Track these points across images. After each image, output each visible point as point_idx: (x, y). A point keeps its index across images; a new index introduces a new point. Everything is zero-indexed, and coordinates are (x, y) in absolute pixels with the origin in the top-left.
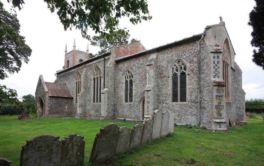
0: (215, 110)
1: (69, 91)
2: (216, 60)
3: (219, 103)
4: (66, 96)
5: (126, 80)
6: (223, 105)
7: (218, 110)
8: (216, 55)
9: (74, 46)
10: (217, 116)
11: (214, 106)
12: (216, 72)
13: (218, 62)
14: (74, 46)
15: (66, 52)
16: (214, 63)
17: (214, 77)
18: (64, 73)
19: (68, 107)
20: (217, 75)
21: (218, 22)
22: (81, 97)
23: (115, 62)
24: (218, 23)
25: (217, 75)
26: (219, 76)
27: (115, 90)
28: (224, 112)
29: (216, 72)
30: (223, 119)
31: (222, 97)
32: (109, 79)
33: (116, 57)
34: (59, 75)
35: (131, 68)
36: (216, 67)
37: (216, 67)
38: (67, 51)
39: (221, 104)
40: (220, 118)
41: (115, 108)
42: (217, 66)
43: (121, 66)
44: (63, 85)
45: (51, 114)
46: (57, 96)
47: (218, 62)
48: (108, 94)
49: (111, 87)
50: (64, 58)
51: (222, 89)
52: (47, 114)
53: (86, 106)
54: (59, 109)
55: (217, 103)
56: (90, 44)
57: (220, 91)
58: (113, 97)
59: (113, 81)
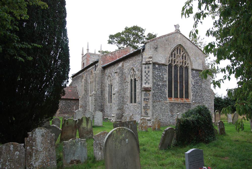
0: (143, 110)
1: (78, 93)
2: (147, 70)
3: (146, 104)
4: (74, 98)
5: (131, 79)
6: (149, 106)
7: (145, 110)
8: (147, 66)
9: (88, 50)
10: (144, 114)
11: (142, 107)
12: (147, 80)
13: (149, 72)
14: (88, 50)
15: (83, 54)
16: (145, 72)
17: (145, 83)
18: (76, 77)
19: (76, 108)
20: (147, 82)
21: (173, 30)
22: (82, 99)
23: (102, 68)
24: (174, 31)
25: (147, 82)
26: (149, 83)
27: (102, 92)
28: (150, 112)
29: (147, 80)
30: (149, 117)
31: (148, 100)
32: (96, 83)
33: (103, 64)
34: (73, 79)
35: (111, 74)
36: (147, 76)
37: (147, 76)
38: (84, 54)
39: (147, 105)
40: (146, 117)
41: (102, 109)
42: (147, 75)
43: (108, 71)
44: (74, 87)
45: (62, 114)
46: (66, 98)
47: (149, 72)
48: (95, 96)
49: (98, 90)
50: (81, 61)
51: (148, 94)
52: (58, 113)
53: (86, 106)
54: (68, 110)
55: (145, 105)
56: (108, 43)
57: (147, 95)
58: (100, 99)
59: (100, 85)
